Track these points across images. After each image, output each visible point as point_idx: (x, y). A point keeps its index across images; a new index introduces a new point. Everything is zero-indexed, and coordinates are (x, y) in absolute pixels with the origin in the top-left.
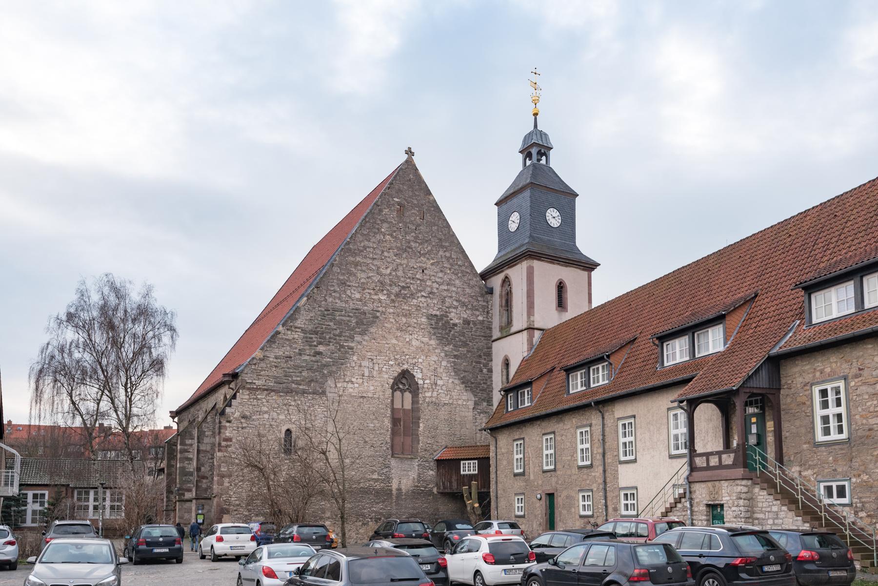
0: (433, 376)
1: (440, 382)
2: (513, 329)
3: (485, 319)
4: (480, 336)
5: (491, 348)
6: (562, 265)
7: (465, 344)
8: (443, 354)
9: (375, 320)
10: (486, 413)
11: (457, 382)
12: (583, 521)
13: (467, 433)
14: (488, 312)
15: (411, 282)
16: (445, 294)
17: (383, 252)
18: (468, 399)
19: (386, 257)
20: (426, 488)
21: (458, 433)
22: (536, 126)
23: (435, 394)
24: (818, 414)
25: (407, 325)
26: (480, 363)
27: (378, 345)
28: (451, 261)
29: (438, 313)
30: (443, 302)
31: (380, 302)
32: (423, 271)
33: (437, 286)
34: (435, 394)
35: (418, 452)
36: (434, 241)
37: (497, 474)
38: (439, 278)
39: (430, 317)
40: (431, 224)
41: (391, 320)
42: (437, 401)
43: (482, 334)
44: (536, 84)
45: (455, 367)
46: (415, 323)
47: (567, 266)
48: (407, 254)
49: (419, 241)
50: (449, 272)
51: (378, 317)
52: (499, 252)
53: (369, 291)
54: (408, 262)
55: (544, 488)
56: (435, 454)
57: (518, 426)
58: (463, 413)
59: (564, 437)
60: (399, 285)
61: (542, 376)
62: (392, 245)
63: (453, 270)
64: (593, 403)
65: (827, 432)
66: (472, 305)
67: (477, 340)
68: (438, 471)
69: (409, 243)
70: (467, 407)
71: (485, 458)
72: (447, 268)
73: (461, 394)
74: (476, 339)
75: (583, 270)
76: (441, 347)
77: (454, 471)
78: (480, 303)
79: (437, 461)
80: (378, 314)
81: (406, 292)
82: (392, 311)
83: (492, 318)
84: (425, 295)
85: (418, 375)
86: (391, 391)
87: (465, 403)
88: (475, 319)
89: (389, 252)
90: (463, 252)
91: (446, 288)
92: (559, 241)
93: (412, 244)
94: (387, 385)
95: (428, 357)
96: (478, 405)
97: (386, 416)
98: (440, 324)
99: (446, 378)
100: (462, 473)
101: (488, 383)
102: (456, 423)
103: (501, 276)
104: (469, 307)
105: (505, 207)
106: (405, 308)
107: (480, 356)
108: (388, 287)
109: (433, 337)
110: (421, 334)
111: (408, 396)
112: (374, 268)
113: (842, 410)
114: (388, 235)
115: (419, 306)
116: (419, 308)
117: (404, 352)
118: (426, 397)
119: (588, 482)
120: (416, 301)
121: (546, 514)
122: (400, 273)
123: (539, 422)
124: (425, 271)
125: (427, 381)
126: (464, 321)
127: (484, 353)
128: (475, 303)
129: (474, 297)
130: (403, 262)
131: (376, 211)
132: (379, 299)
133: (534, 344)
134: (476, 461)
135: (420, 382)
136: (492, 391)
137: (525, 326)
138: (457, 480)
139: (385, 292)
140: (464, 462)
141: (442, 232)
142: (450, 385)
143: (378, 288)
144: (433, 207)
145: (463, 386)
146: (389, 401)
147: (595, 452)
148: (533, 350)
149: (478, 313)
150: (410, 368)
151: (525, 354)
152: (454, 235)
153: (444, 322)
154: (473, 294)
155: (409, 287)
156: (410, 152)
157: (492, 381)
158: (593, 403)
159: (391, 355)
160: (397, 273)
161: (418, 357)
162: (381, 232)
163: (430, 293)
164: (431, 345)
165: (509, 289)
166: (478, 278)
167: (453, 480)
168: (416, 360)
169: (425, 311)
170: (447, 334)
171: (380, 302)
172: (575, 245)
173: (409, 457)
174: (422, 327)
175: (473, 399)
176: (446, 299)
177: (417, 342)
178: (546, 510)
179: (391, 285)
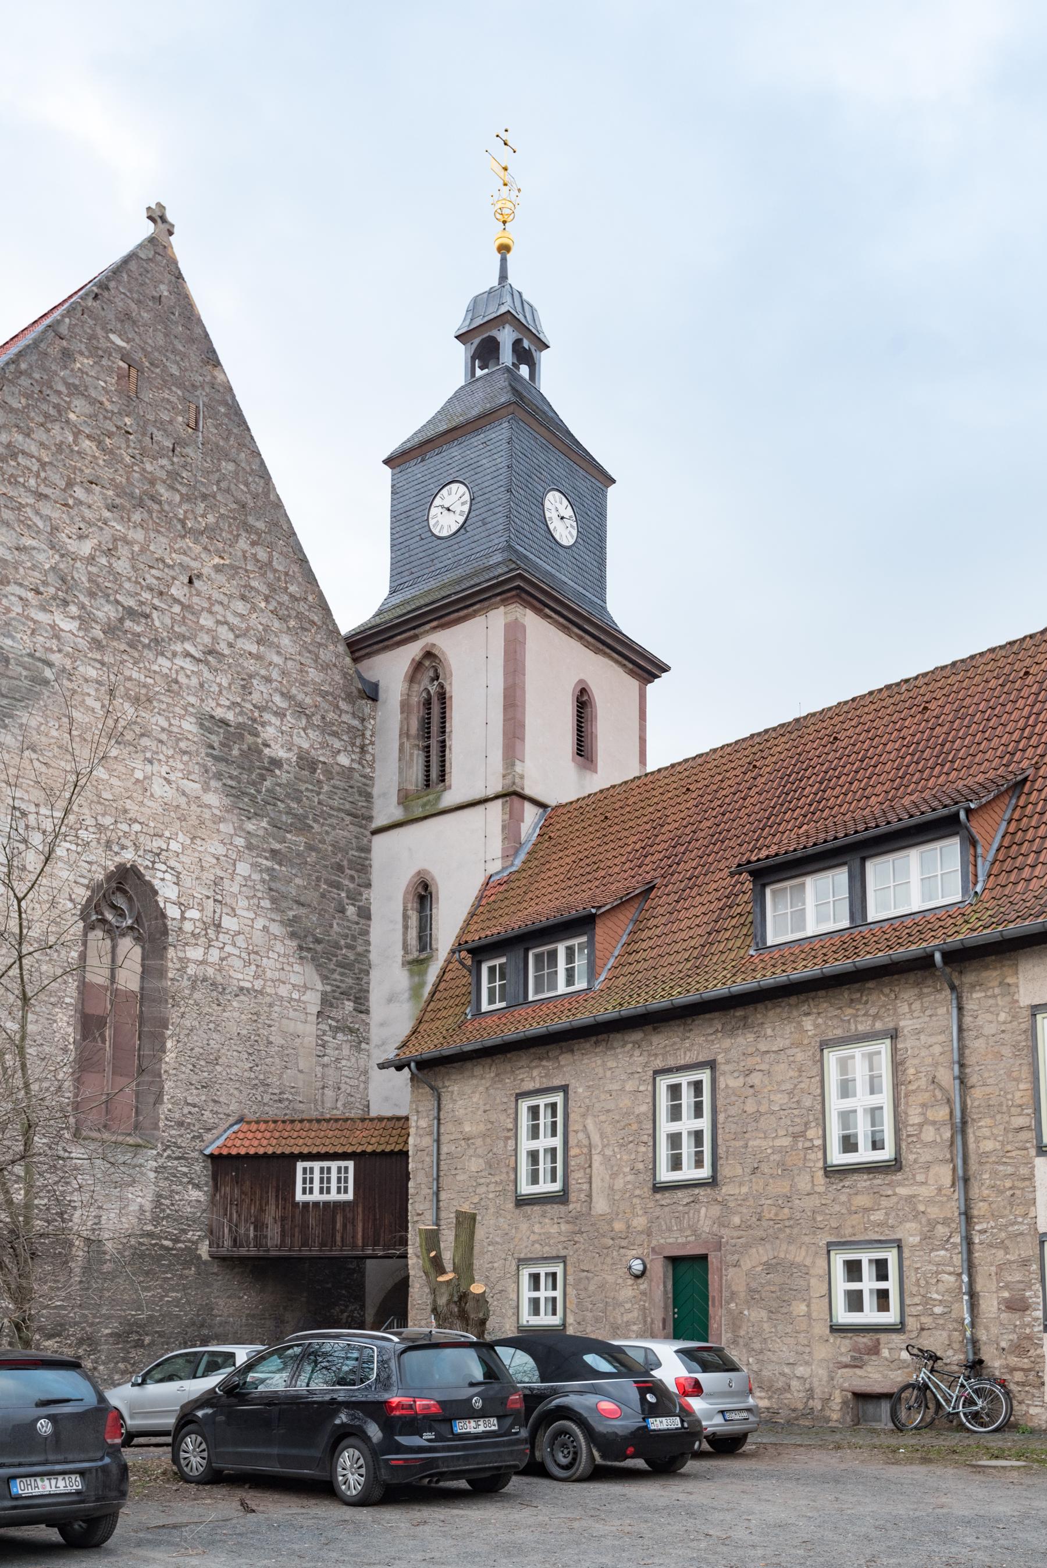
0: (211, 901)
1: (229, 923)
2: (449, 799)
3: (355, 766)
4: (339, 810)
5: (367, 850)
6: (587, 645)
7: (301, 826)
8: (240, 842)
9: (38, 688)
10: (351, 1031)
11: (276, 929)
12: (844, 1345)
13: (300, 1084)
14: (363, 749)
15: (156, 601)
16: (251, 665)
17: (70, 484)
18: (305, 986)
19: (81, 503)
20: (176, 1241)
21: (273, 1080)
22: (503, 277)
23: (214, 955)
24: (663, 1130)
25: (138, 730)
26: (338, 886)
27: (44, 769)
28: (270, 575)
29: (230, 716)
30: (246, 689)
31: (58, 638)
32: (191, 581)
33: (231, 637)
34: (214, 955)
35: (156, 1127)
36: (226, 505)
37: (438, 1201)
38: (236, 614)
39: (209, 722)
40: (220, 454)
41: (90, 702)
42: (219, 979)
43: (348, 806)
44: (505, 169)
45: (273, 885)
46: (163, 729)
47: (597, 651)
48: (146, 515)
49: (184, 490)
50: (263, 605)
51: (46, 682)
52: (393, 591)
53: (23, 593)
54: (148, 541)
55: (657, 1240)
56: (208, 1137)
57: (541, 1050)
58: (292, 1024)
59: (756, 1079)
60: (117, 602)
61: (624, 903)
62: (100, 472)
63: (274, 604)
64: (938, 956)
65: (676, 1163)
66: (323, 718)
67: (334, 821)
68: (216, 1188)
69: (152, 483)
70: (300, 1006)
71: (383, 1153)
72: (258, 591)
73: (287, 968)
74: (331, 816)
75: (631, 673)
76: (235, 819)
77: (272, 1195)
78: (345, 718)
79: (215, 1159)
80: (48, 673)
81: (138, 629)
82: (92, 673)
83: (371, 767)
84: (197, 656)
85: (167, 891)
86: (81, 924)
87: (296, 995)
88: (331, 761)
89: (88, 491)
90: (303, 561)
91: (253, 648)
92: (572, 584)
93: (161, 489)
94: (70, 905)
95: (198, 841)
96: (331, 1006)
97: (59, 1003)
98: (235, 752)
99: (245, 913)
100: (299, 1197)
101: (360, 949)
102: (273, 1050)
103: (413, 651)
104: (316, 720)
105: (416, 470)
106: (135, 675)
107: (340, 868)
108: (82, 598)
109: (213, 783)
110: (181, 766)
111: (130, 950)
112: (40, 524)
113: (704, 1124)
114: (88, 437)
115: (176, 682)
116: (175, 687)
117: (126, 811)
118: (189, 960)
119: (877, 1216)
120: (167, 663)
121: (664, 1321)
122: (122, 566)
123: (637, 1036)
124: (197, 583)
125: (193, 914)
126: (300, 758)
127: (349, 861)
128: (331, 716)
129: (330, 698)
130: (131, 535)
131: (54, 351)
132: (53, 626)
133: (523, 839)
134: (350, 1164)
135: (173, 912)
136: (368, 973)
137: (496, 786)
138: (283, 1219)
139: (73, 609)
140: (308, 1164)
141: (247, 485)
142: (258, 937)
143: (52, 590)
144: (225, 403)
145: (294, 944)
146: (74, 954)
147: (915, 1119)
148: (522, 856)
149: (337, 744)
150: (142, 864)
151: (496, 866)
152: (278, 505)
153: (245, 747)
154: (326, 688)
155: (147, 616)
156: (157, 216)
157: (368, 943)
158: (938, 956)
159: (86, 811)
160: (113, 560)
161: (167, 834)
162: (68, 421)
163: (211, 652)
164: (209, 807)
165: (433, 689)
166: (341, 648)
167: (269, 1220)
168: (158, 843)
169: (192, 700)
170: (254, 784)
171: (58, 638)
172: (604, 609)
173: (131, 1140)
174: (183, 745)
175: (319, 986)
176: (255, 682)
177: (167, 788)
178: (666, 1308)
179: (92, 595)
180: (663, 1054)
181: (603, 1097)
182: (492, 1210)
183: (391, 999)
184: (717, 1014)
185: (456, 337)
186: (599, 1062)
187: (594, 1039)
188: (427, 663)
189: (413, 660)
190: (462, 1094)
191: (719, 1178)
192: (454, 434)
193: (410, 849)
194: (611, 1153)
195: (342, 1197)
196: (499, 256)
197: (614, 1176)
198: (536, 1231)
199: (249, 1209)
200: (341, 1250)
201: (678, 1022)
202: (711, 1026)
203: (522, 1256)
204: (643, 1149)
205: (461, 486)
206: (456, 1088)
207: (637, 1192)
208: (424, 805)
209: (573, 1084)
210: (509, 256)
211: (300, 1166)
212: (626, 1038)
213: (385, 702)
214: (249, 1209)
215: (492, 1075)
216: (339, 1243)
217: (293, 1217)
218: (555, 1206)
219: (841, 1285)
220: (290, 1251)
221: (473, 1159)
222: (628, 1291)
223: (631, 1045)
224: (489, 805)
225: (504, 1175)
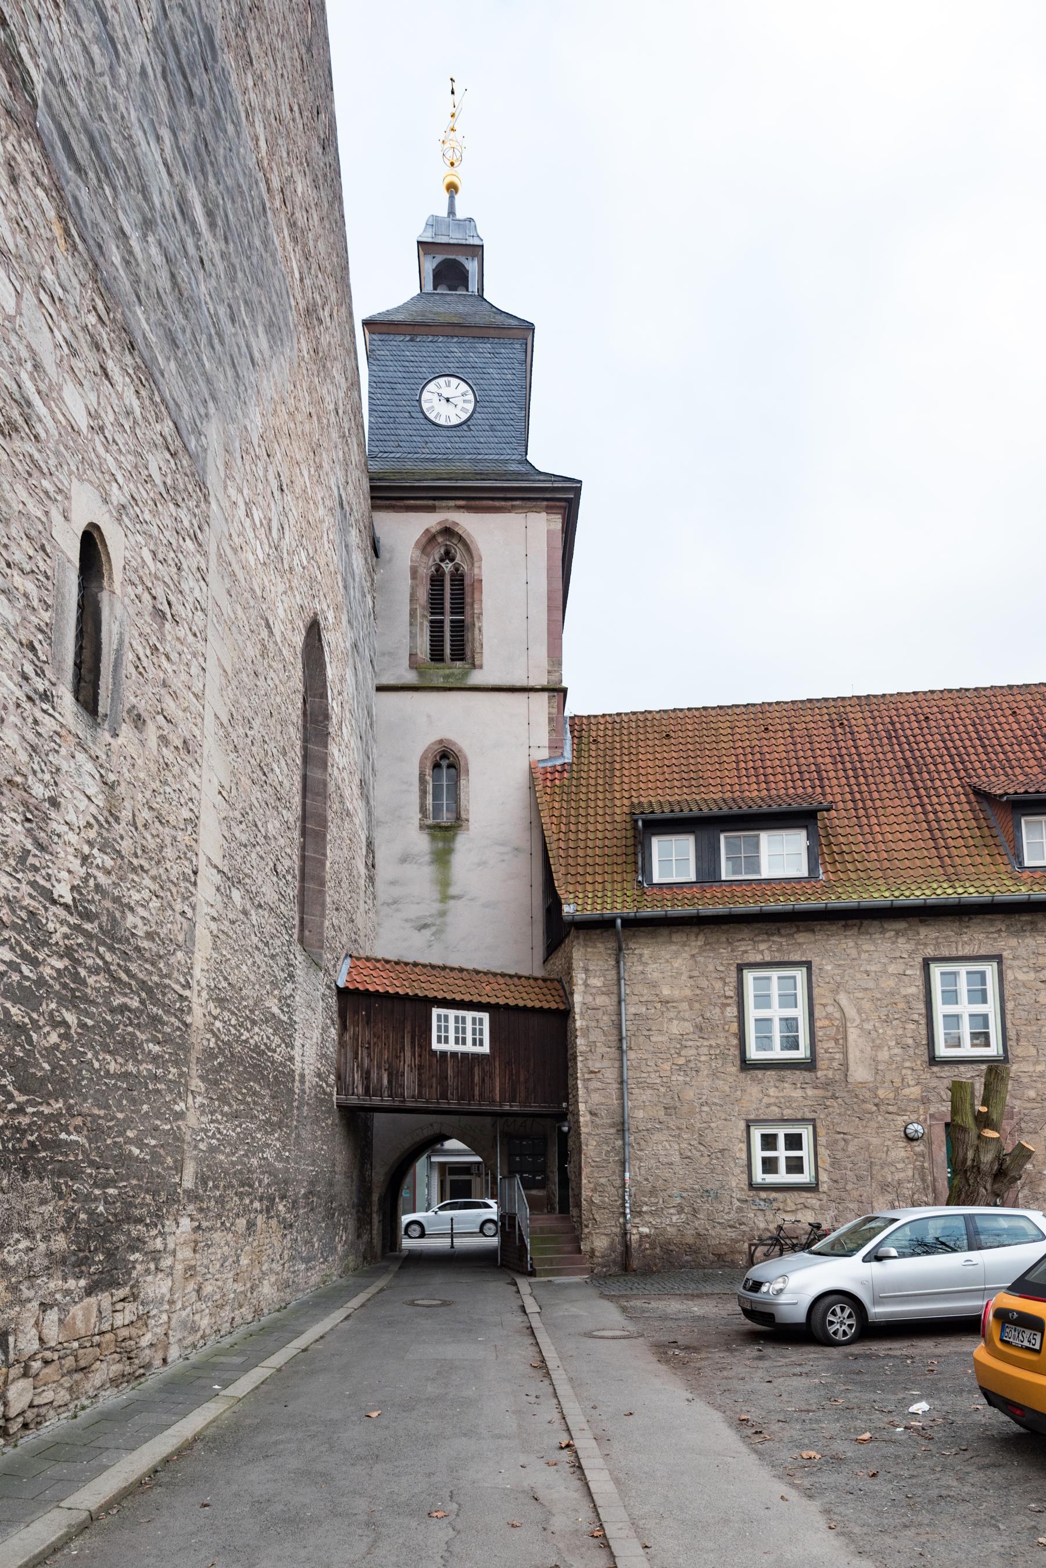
2: (477, 678)
24: (939, 1011)
57: (773, 927)
64: (619, 921)
68: (343, 1028)
79: (343, 993)
100: (435, 1046)
103: (431, 521)
123: (902, 925)
134: (486, 1017)
140: (443, 1011)
158: (619, 921)
180: (934, 945)
181: (858, 976)
182: (706, 1072)
183: (405, 859)
184: (1000, 916)
185: (419, 243)
186: (851, 944)
187: (843, 923)
188: (440, 540)
189: (427, 530)
190: (655, 959)
191: (1010, 1056)
192: (457, 331)
193: (429, 716)
194: (871, 1027)
195: (478, 1049)
196: (447, 196)
197: (877, 1048)
198: (772, 1094)
199: (381, 1053)
200: (480, 1105)
201: (950, 918)
202: (992, 926)
203: (752, 1117)
204: (911, 1026)
205: (462, 384)
206: (646, 952)
207: (907, 1064)
208: (446, 677)
209: (816, 961)
210: (457, 197)
211: (435, 1011)
212: (886, 926)
213: (390, 560)
214: (381, 1053)
215: (699, 943)
216: (477, 1097)
217: (430, 1066)
218: (798, 1072)
219: (759, 1154)
220: (427, 1102)
221: (675, 1022)
222: (900, 1151)
223: (893, 933)
224: (532, 695)
225: (723, 1040)
